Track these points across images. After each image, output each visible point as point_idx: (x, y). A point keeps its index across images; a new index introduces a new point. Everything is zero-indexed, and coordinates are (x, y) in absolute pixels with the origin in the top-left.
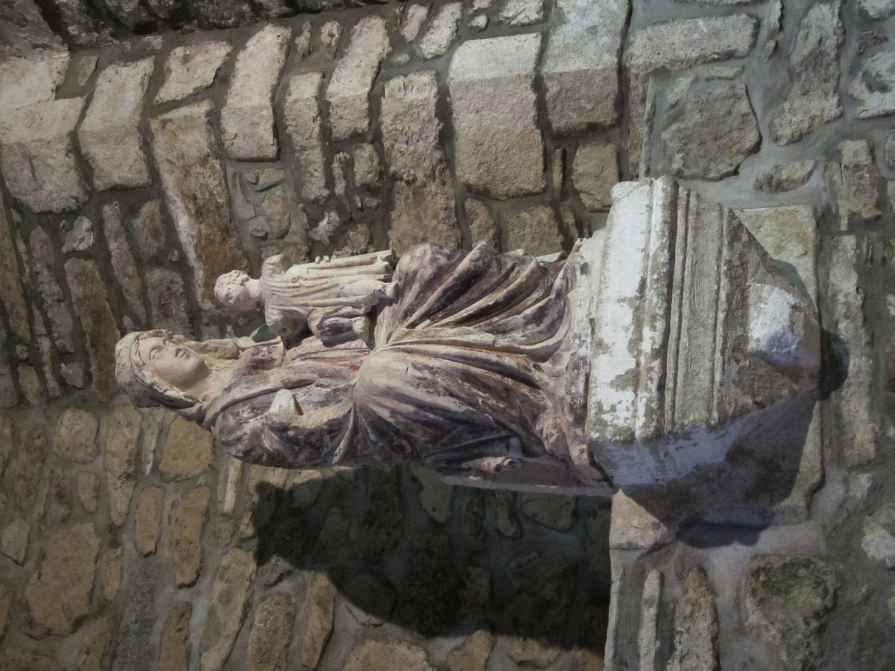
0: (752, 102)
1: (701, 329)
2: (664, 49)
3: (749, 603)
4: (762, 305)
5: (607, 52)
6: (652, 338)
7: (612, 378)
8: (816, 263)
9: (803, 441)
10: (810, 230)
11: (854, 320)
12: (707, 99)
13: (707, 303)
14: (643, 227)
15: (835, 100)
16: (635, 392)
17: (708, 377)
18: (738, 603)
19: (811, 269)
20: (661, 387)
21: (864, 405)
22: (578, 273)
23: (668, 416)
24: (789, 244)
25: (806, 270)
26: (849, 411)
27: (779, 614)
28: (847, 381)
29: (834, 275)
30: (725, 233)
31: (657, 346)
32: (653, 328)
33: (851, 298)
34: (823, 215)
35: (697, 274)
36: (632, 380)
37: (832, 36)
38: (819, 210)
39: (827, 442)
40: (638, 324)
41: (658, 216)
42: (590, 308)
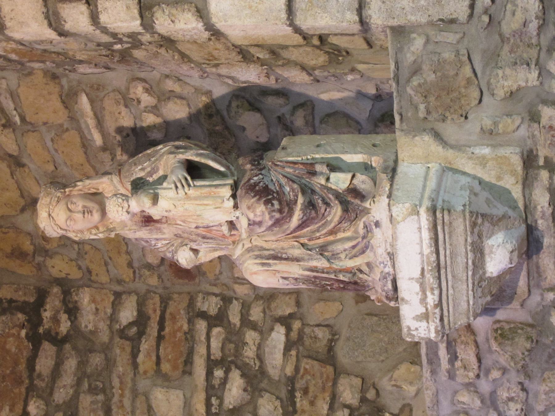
0: (473, 63)
1: (460, 282)
2: (397, 13)
3: (492, 342)
4: (493, 255)
5: (348, 10)
6: (433, 299)
7: (413, 315)
8: (524, 188)
9: (518, 280)
10: (519, 168)
11: (547, 220)
12: (438, 61)
13: (461, 269)
14: (418, 241)
15: (537, 72)
16: (428, 322)
17: (466, 304)
18: (487, 340)
19: (521, 192)
20: (442, 319)
21: (552, 262)
22: (374, 227)
23: (447, 327)
24: (506, 176)
25: (517, 192)
26: (544, 264)
27: (509, 348)
28: (543, 251)
29: (535, 194)
30: (468, 229)
31: (436, 302)
32: (433, 294)
33: (545, 209)
34: (528, 156)
35: (454, 256)
36: (426, 317)
37: (534, 20)
38: (525, 153)
39: (531, 278)
40: (424, 292)
41: (426, 235)
42: (386, 246)
